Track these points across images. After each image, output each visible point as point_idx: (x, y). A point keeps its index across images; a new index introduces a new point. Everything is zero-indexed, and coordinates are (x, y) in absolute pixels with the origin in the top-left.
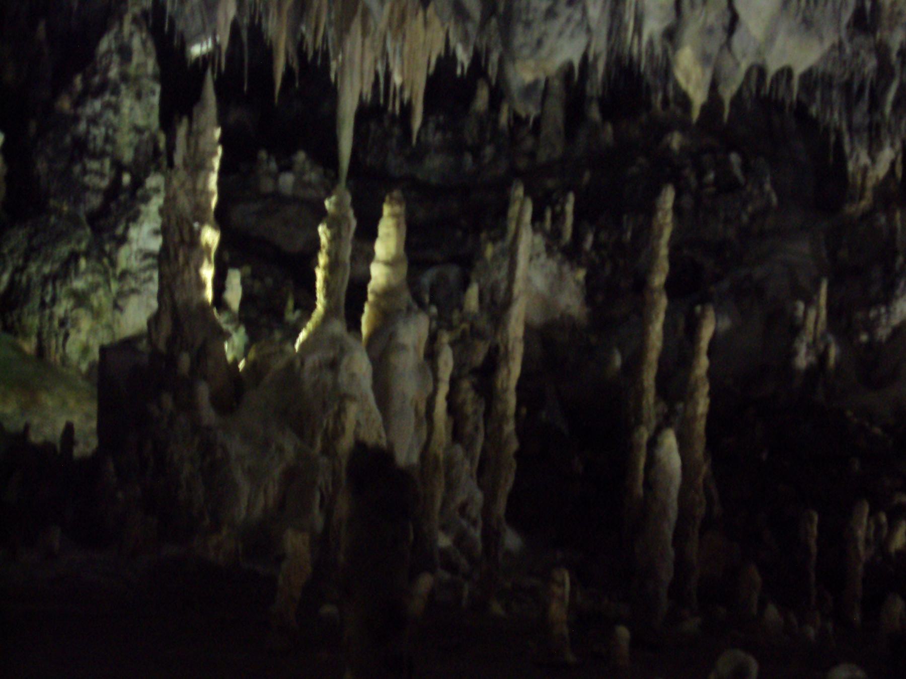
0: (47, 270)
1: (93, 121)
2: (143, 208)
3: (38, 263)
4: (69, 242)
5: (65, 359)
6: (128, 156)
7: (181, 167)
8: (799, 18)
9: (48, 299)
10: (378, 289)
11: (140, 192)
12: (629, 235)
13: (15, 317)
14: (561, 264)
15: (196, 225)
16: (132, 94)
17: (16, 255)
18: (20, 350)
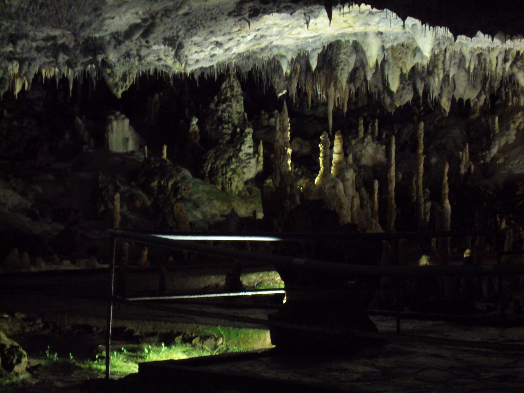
0: (222, 163)
1: (223, 111)
2: (245, 139)
3: (219, 161)
4: (228, 154)
5: (231, 190)
6: (236, 122)
7: (279, 131)
8: (472, 85)
9: (224, 172)
10: (336, 162)
11: (244, 134)
12: (396, 131)
13: (215, 179)
14: (377, 144)
15: (286, 148)
16: (236, 102)
17: (212, 159)
18: (218, 189)
